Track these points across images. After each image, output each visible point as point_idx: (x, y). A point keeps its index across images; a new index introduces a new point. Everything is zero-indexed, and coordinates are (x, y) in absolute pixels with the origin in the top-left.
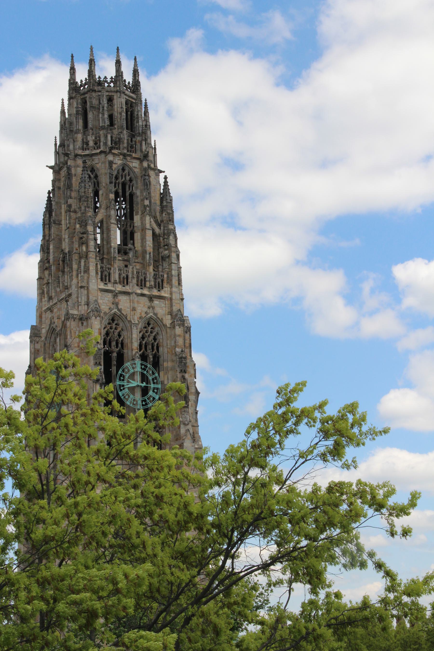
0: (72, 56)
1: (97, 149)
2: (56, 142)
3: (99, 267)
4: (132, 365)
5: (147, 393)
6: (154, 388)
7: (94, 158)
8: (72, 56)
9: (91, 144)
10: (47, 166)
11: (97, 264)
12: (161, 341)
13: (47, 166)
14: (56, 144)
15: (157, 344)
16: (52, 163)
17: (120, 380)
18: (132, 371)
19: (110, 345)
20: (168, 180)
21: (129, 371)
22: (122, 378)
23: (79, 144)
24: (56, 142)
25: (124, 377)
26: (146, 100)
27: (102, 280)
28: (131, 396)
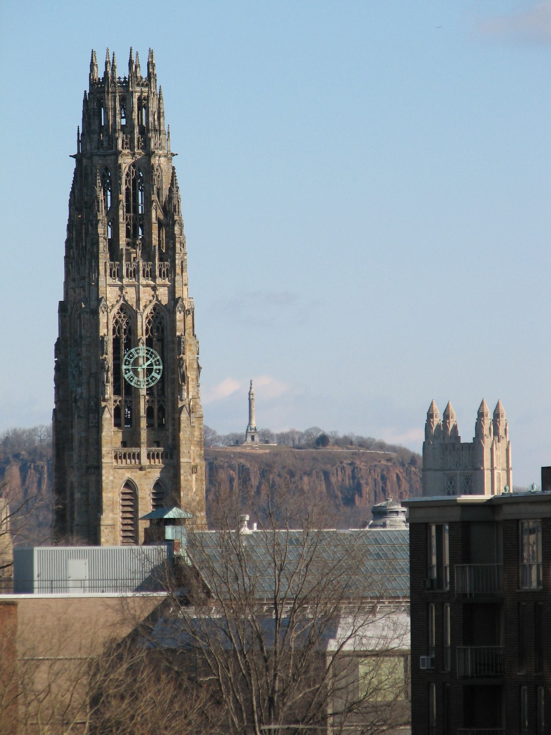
0: (131, 50)
1: (110, 150)
2: (78, 131)
3: (108, 264)
4: (136, 350)
5: (150, 373)
6: (156, 369)
7: (107, 158)
8: (131, 50)
9: (105, 144)
10: (70, 156)
11: (106, 263)
12: (165, 324)
13: (70, 156)
14: (78, 133)
15: (162, 327)
16: (75, 152)
17: (125, 364)
18: (136, 356)
19: (119, 333)
20: (176, 171)
21: (133, 356)
22: (127, 363)
23: (95, 144)
24: (78, 131)
25: (129, 362)
26: (137, 54)
27: (111, 276)
28: (136, 378)
